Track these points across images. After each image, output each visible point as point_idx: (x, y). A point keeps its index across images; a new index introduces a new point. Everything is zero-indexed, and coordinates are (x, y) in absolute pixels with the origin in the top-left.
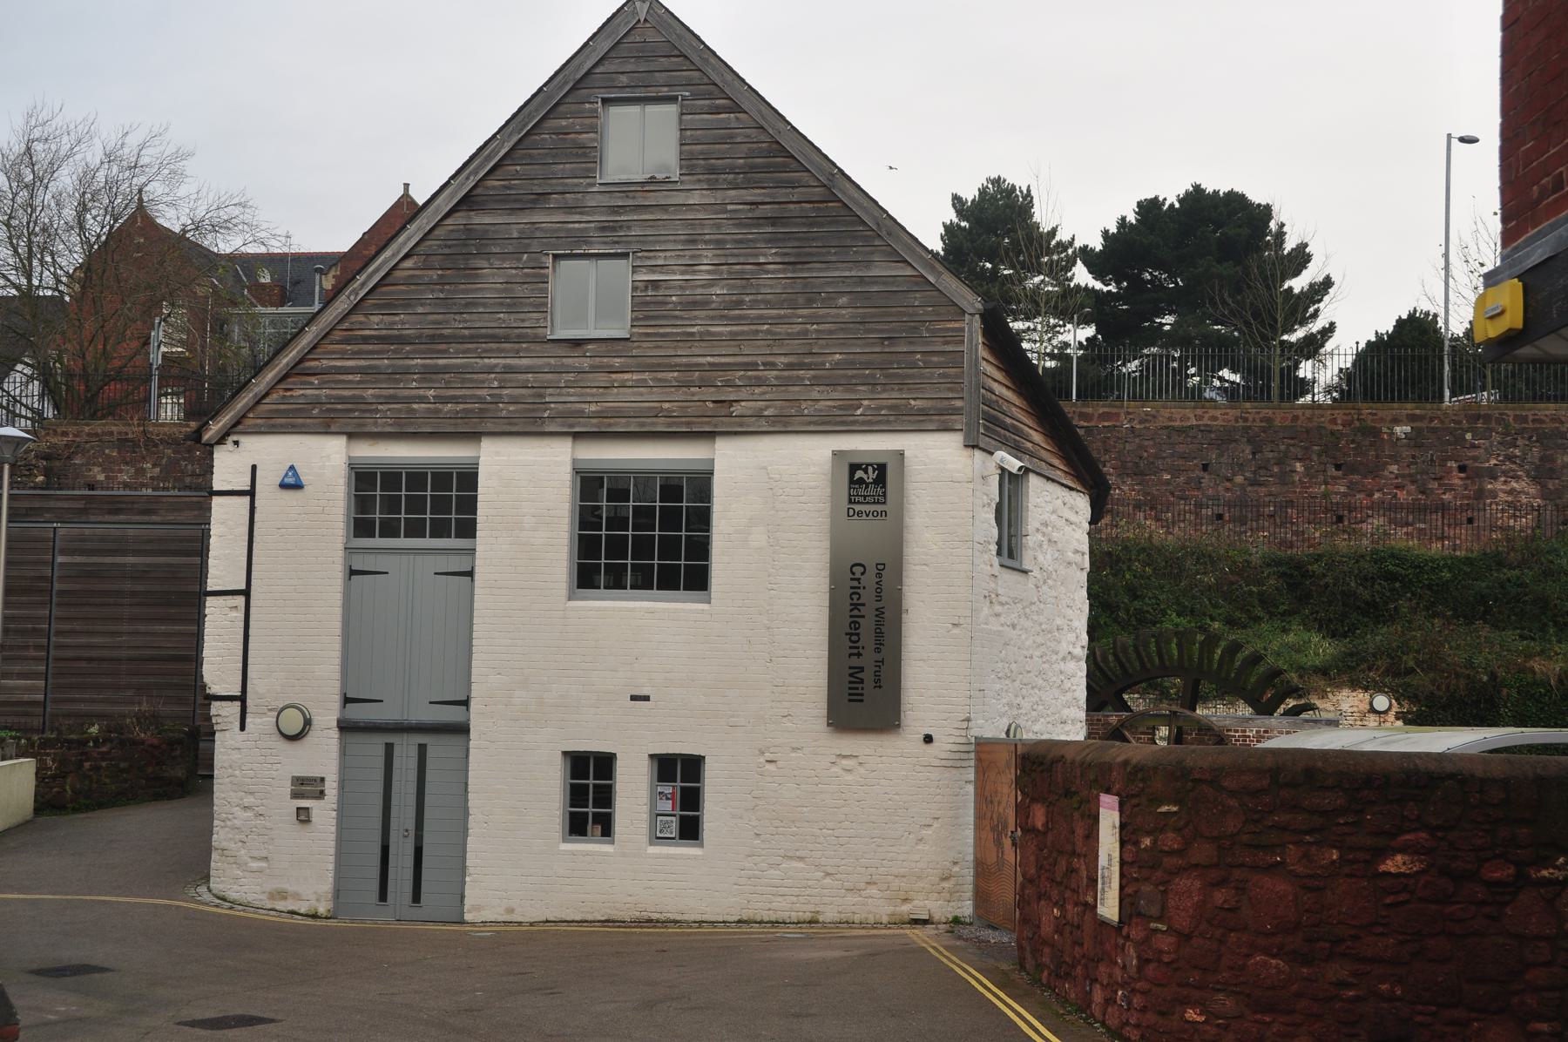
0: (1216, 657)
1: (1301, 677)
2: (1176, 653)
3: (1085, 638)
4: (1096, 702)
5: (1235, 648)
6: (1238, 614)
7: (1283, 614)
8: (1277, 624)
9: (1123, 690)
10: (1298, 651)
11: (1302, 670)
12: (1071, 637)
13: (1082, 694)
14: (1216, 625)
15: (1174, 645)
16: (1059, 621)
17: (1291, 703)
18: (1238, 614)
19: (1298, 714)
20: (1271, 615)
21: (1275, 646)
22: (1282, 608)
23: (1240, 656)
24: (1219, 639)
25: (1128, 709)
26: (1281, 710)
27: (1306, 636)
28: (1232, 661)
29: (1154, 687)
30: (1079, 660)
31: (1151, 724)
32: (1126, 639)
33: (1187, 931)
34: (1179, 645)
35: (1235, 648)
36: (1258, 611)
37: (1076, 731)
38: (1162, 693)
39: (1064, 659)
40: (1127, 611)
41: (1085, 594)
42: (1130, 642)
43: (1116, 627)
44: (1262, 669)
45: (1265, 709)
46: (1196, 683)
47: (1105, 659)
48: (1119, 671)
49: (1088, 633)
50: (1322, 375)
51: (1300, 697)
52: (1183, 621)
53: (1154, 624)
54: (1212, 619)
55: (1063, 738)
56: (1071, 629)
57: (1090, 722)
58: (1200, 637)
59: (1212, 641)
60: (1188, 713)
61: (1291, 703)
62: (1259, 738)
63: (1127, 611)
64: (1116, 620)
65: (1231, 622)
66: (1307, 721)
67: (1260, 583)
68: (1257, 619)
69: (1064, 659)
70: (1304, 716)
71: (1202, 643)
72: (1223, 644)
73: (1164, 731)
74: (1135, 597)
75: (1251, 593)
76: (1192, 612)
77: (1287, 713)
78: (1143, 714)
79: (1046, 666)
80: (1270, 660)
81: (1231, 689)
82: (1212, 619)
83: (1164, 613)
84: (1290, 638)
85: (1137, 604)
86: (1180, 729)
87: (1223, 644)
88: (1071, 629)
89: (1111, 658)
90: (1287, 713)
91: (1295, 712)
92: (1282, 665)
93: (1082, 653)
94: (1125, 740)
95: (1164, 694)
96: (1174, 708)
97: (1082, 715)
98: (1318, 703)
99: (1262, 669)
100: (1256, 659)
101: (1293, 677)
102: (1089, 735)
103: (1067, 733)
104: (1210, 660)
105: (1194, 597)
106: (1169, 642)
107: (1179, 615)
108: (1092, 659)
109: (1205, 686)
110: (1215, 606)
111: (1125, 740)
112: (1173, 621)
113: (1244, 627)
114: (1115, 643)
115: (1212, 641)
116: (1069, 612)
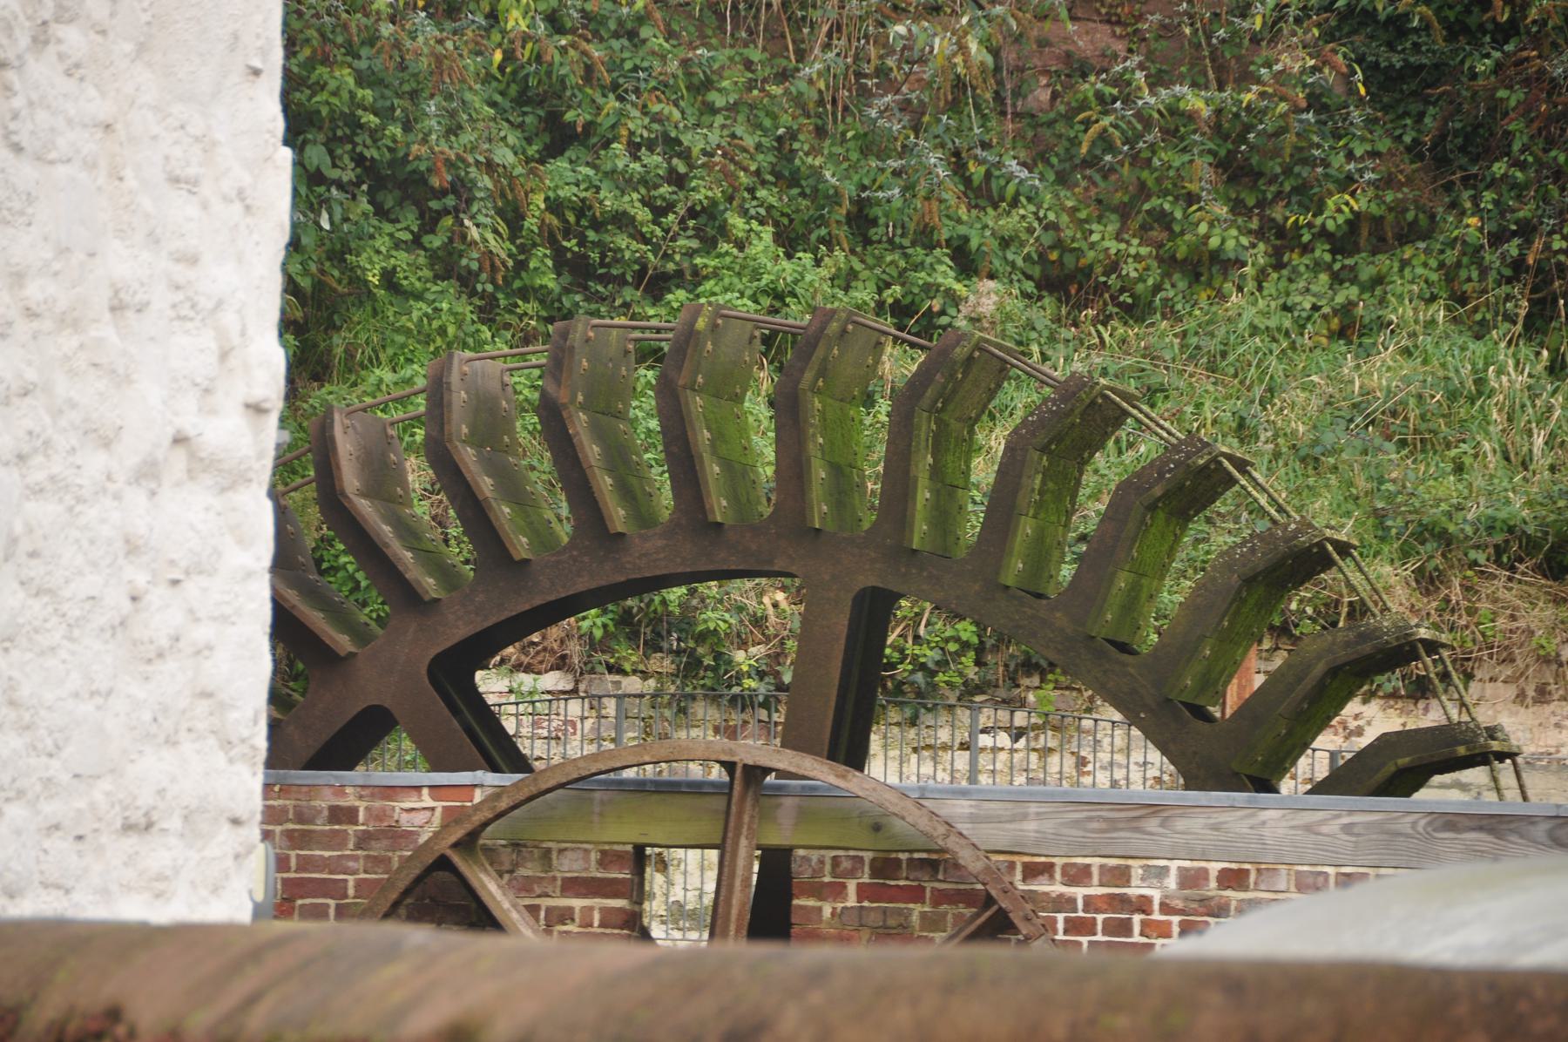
0: (983, 472)
1: (1427, 581)
2: (765, 449)
3: (266, 361)
4: (322, 713)
5: (1082, 422)
6: (1104, 238)
7: (1344, 242)
8: (1314, 290)
9: (480, 649)
10: (1419, 443)
11: (1432, 546)
12: (193, 350)
13: (246, 666)
14: (987, 297)
15: (757, 409)
16: (122, 263)
17: (1370, 720)
18: (1104, 238)
19: (1405, 782)
20: (1283, 241)
21: (1296, 414)
22: (1338, 209)
23: (1108, 469)
24: (1002, 371)
25: (500, 751)
26: (1314, 763)
27: (1461, 357)
28: (1064, 488)
29: (647, 633)
30: (236, 480)
31: (623, 834)
32: (499, 369)
33: (1006, 234)
34: (787, 407)
35: (1082, 422)
36: (1216, 225)
37: (214, 876)
38: (691, 667)
39: (148, 473)
40: (513, 217)
41: (266, 109)
42: (525, 385)
43: (450, 303)
44: (1219, 536)
45: (1235, 757)
46: (874, 610)
47: (383, 479)
48: (459, 552)
49: (287, 325)
50: (961, 553)
51: (1421, 690)
52: (810, 274)
53: (656, 285)
54: (967, 263)
55: (133, 909)
56: (191, 310)
57: (288, 828)
58: (898, 364)
59: (958, 381)
60: (822, 772)
61: (1370, 720)
62: (1200, 910)
63: (513, 217)
64: (446, 266)
65: (1064, 282)
66: (1451, 822)
67: (1228, 70)
68: (1205, 268)
69: (148, 473)
70: (1439, 793)
71: (908, 398)
72: (1020, 399)
73: (689, 877)
74: (559, 138)
75: (1176, 123)
76: (861, 219)
77: (1345, 779)
78: (585, 785)
79: (46, 511)
80: (1269, 483)
81: (1055, 646)
82: (967, 263)
83: (708, 225)
84: (1380, 372)
85: (565, 176)
86: (776, 863)
87: (1020, 399)
88: (191, 310)
89: (417, 473)
90: (1345, 779)
91: (1393, 771)
92: (1327, 515)
93: (257, 444)
94: (482, 918)
95: (701, 671)
96: (754, 749)
97: (244, 782)
98: (1518, 725)
99: (1219, 536)
100: (1192, 486)
101: (1388, 587)
102: (289, 897)
103: (159, 885)
104: (949, 487)
105: (871, 145)
106: (729, 389)
107: (789, 241)
108: (308, 471)
109: (920, 632)
110: (983, 195)
111: (482, 918)
112: (756, 273)
113: (1136, 311)
114: (438, 391)
115: (958, 381)
116: (181, 209)
